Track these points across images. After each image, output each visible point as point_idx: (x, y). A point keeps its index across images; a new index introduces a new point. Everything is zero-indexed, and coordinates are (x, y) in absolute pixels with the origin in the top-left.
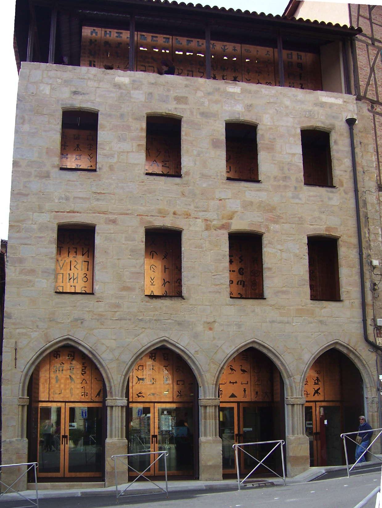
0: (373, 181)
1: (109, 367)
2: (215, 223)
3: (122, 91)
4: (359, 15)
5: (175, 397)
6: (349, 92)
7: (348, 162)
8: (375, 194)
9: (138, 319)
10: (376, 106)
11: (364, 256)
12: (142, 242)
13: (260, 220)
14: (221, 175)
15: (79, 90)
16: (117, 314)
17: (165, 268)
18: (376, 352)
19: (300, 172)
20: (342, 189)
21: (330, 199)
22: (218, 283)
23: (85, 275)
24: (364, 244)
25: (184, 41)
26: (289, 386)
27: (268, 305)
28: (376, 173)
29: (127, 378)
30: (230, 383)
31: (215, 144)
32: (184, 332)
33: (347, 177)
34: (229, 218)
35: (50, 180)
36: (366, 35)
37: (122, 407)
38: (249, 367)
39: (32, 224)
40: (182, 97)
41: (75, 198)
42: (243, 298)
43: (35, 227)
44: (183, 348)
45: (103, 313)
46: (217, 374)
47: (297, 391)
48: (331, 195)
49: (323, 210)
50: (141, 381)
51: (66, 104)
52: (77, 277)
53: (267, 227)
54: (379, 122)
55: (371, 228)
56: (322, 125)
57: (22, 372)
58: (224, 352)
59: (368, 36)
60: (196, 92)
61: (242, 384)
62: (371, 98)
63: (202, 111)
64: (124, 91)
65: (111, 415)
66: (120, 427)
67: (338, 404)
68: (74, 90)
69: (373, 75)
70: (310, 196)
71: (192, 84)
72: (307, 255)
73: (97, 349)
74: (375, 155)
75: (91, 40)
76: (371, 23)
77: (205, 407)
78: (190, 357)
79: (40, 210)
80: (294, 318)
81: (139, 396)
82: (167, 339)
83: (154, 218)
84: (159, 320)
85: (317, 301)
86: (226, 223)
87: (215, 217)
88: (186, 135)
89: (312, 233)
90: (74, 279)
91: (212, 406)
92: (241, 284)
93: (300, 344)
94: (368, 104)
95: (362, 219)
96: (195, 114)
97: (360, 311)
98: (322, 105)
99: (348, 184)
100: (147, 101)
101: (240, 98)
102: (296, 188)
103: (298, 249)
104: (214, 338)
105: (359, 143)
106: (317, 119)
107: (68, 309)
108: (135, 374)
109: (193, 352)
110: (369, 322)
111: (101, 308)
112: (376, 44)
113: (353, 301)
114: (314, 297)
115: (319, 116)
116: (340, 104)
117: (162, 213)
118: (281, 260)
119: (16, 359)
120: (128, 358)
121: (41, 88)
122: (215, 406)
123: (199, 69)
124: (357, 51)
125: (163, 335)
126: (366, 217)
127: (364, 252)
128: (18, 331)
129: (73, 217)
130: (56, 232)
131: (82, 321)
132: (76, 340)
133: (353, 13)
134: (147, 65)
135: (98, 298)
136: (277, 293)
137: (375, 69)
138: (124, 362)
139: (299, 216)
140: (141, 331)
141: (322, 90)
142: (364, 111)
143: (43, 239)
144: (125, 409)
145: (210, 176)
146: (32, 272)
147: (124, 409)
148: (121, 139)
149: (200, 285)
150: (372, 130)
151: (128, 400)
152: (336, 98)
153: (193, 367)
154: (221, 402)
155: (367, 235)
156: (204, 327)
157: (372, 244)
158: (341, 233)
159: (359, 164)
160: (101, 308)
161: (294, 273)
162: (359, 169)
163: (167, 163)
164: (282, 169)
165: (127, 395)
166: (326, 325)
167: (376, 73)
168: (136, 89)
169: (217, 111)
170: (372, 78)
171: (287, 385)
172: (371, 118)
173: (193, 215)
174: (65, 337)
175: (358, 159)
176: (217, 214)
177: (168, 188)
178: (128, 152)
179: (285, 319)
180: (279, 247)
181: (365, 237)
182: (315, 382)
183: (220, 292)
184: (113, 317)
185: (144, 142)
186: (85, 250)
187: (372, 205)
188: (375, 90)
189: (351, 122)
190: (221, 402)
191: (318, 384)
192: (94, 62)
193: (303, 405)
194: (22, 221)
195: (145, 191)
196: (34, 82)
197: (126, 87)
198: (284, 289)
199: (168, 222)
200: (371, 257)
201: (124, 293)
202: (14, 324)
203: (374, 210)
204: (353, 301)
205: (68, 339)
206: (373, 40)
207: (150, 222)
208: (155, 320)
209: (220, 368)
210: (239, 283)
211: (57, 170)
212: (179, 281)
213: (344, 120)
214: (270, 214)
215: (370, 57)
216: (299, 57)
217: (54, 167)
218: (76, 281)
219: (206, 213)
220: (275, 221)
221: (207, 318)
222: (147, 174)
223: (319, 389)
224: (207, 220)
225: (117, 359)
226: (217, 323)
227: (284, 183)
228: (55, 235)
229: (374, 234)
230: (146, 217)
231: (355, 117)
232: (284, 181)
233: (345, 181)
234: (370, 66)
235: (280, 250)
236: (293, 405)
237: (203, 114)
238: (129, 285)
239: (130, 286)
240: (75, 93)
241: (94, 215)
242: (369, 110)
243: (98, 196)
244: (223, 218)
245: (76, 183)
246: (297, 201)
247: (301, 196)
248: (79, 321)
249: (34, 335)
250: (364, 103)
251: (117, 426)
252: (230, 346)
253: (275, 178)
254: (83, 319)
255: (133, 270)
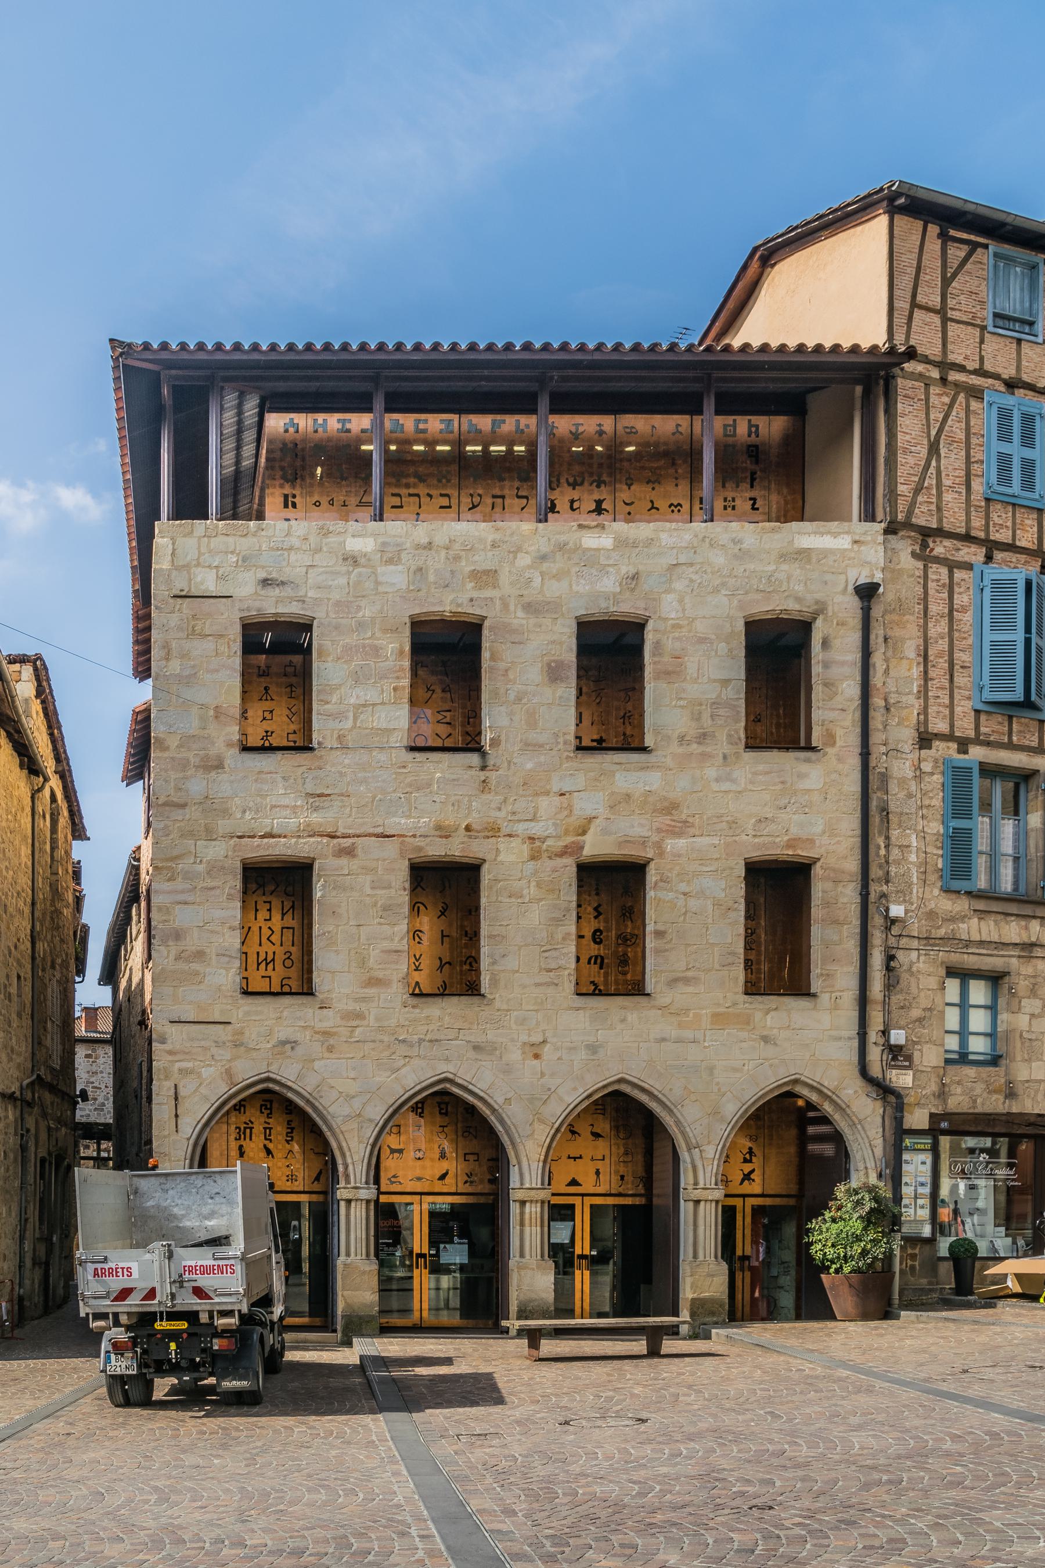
0: (907, 726)
1: (344, 1129)
2: (549, 842)
3: (360, 570)
4: (914, 305)
5: (460, 1184)
6: (869, 515)
7: (851, 689)
8: (909, 756)
9: (396, 1039)
10: (934, 542)
11: (872, 897)
12: (405, 889)
13: (646, 833)
14: (565, 743)
15: (274, 575)
16: (358, 1031)
17: (443, 936)
18: (884, 1099)
19: (737, 721)
20: (831, 751)
21: (801, 776)
22: (553, 966)
23: (288, 955)
24: (875, 872)
25: (484, 422)
26: (690, 1166)
27: (654, 1007)
28: (917, 706)
29: (377, 1149)
30: (569, 1157)
31: (554, 673)
32: (484, 1063)
33: (848, 723)
34: (580, 831)
35: (225, 772)
36: (926, 356)
37: (368, 1201)
38: (607, 1127)
39: (195, 863)
40: (487, 572)
41: (273, 807)
42: (601, 994)
43: (201, 868)
44: (482, 1094)
45: (334, 1030)
46: (548, 1140)
47: (708, 1175)
48: (804, 768)
49: (783, 802)
50: (396, 1155)
51: (248, 609)
52: (273, 960)
53: (659, 846)
54: (938, 581)
55: (894, 833)
56: (797, 607)
57: (189, 1139)
58: (561, 1099)
59: (932, 358)
60: (515, 558)
61: (592, 1159)
62: (923, 524)
63: (526, 600)
64: (364, 570)
65: (348, 1215)
66: (364, 1236)
67: (792, 1202)
68: (263, 575)
69: (934, 463)
70: (755, 774)
71: (506, 539)
72: (743, 900)
73: (321, 1097)
74: (919, 664)
75: (285, 444)
76: (945, 320)
77: (523, 1203)
78: (494, 1110)
79: (210, 835)
80: (708, 1033)
81: (392, 1183)
82: (451, 1076)
83: (428, 840)
84: (437, 1041)
85: (757, 997)
86: (573, 842)
87: (551, 831)
88: (493, 658)
89: (755, 854)
90: (267, 964)
91: (537, 1201)
92: (595, 963)
93: (718, 1084)
94: (914, 540)
95: (875, 819)
96: (512, 608)
97: (855, 1014)
98: (804, 555)
99: (848, 736)
100: (411, 588)
101: (611, 562)
102: (725, 757)
103: (724, 890)
104: (543, 1074)
105: (881, 640)
106: (786, 594)
107: (267, 1023)
108: (392, 1141)
109: (500, 1100)
110: (873, 1036)
111: (328, 1020)
112: (954, 376)
113: (838, 994)
114: (752, 989)
115: (792, 586)
116: (846, 550)
117: (444, 832)
118: (685, 914)
119: (177, 1116)
120: (378, 1112)
121: (199, 579)
122: (543, 1202)
123: (518, 489)
124: (899, 406)
125: (444, 1069)
126: (884, 809)
127: (875, 889)
128: (177, 1065)
129: (269, 846)
130: (239, 877)
131: (294, 1044)
132: (283, 1081)
133: (897, 304)
134: (404, 492)
135: (322, 1002)
136: (673, 982)
137: (941, 446)
138: (371, 1120)
139: (729, 818)
140: (402, 1062)
141: (802, 520)
142: (903, 560)
143: (218, 892)
144: (372, 1204)
145: (541, 746)
146: (200, 955)
147: (372, 1206)
148: (358, 678)
149: (517, 971)
150: (919, 604)
151: (378, 1189)
152: (835, 535)
153: (499, 1128)
154: (553, 1195)
155: (883, 852)
156: (524, 1053)
157: (893, 869)
158: (823, 850)
159: (878, 689)
160: (328, 1020)
161: (711, 941)
162: (877, 701)
163: (448, 714)
164: (697, 718)
165: (377, 1181)
166: (775, 1044)
167: (943, 455)
168: (390, 561)
169: (560, 597)
170: (932, 470)
171: (684, 1162)
172: (917, 573)
173: (505, 830)
174: (263, 1076)
175: (877, 679)
176: (554, 824)
177: (454, 777)
178: (374, 705)
179: (688, 1034)
180: (683, 887)
181: (878, 855)
182: (745, 1159)
183: (557, 985)
184: (351, 1037)
185: (406, 682)
186: (288, 905)
187: (902, 781)
188: (934, 500)
189: (867, 593)
190: (553, 1195)
191: (750, 1161)
192: (294, 496)
193: (717, 1202)
194: (177, 857)
195: (410, 785)
196: (184, 566)
197: (369, 560)
198: (690, 974)
199: (455, 849)
200: (888, 901)
201: (371, 991)
202: (170, 1053)
203: (905, 792)
204: (838, 994)
205: (268, 1079)
206: (945, 366)
207: (420, 849)
208: (431, 1041)
209: (553, 1131)
210: (593, 961)
211: (235, 751)
212: (473, 961)
213: (851, 588)
214: (667, 820)
215: (932, 417)
216: (753, 429)
217: (230, 745)
218: (271, 966)
219: (533, 824)
220: (681, 829)
221: (529, 1035)
222: (413, 749)
223: (753, 1171)
224: (533, 839)
225: (359, 1115)
226: (548, 1045)
227: (701, 749)
228: (238, 884)
229: (900, 847)
230: (412, 839)
231: (878, 577)
232: (699, 743)
233: (839, 733)
234: (929, 436)
235: (685, 894)
236: (697, 1202)
237: (530, 608)
238: (380, 974)
239: (381, 976)
240: (266, 582)
241: (312, 840)
242: (914, 555)
243: (318, 801)
244: (567, 832)
245: (274, 776)
246: (726, 786)
247: (736, 774)
248: (288, 1046)
249: (207, 1073)
250: (903, 538)
251: (359, 1235)
252: (575, 1089)
253: (682, 739)
254: (295, 1042)
255: (386, 945)
